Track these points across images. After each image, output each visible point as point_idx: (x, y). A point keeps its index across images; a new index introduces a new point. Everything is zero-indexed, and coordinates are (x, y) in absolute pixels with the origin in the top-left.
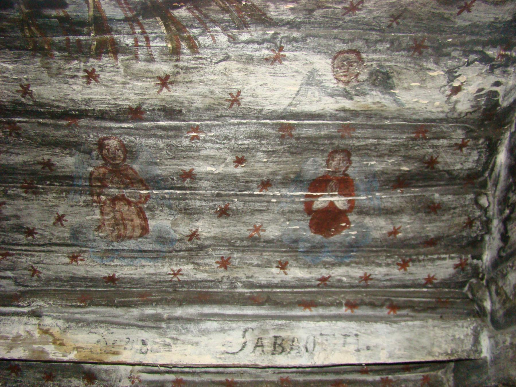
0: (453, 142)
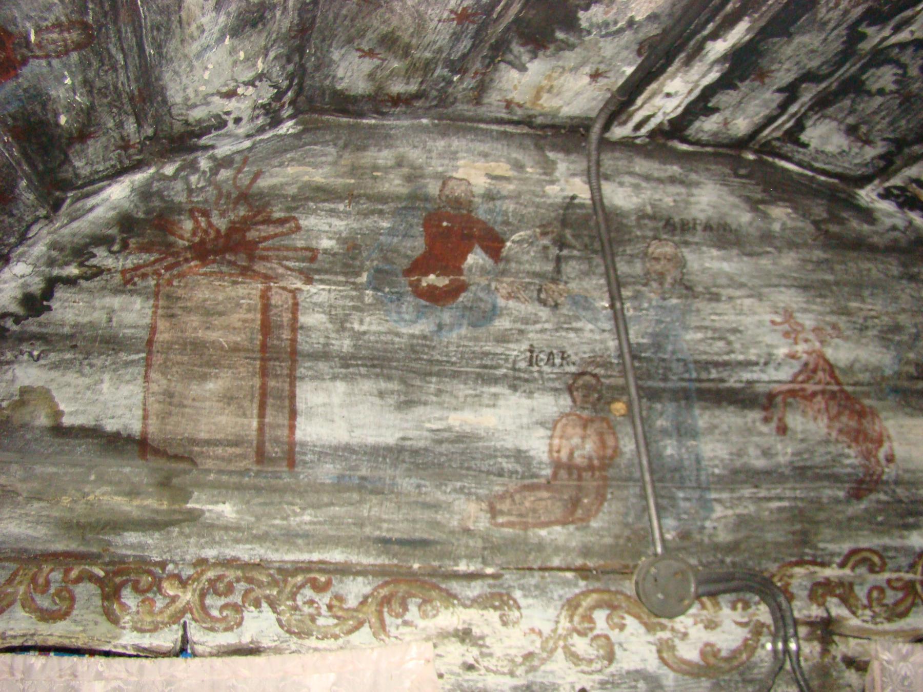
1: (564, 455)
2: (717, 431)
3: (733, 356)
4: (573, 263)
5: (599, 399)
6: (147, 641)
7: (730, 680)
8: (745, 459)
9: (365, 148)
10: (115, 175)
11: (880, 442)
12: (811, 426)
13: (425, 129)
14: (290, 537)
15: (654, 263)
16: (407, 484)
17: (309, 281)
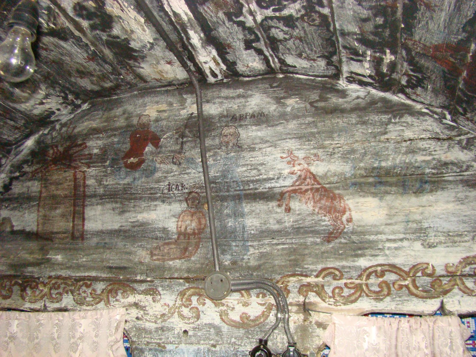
0: (16, 125)
1: (183, 229)
2: (254, 213)
3: (261, 176)
4: (188, 144)
5: (198, 203)
6: (33, 306)
7: (254, 330)
8: (268, 225)
9: (112, 109)
10: (27, 137)
11: (344, 212)
12: (304, 207)
13: (136, 96)
14: (79, 267)
15: (224, 138)
16: (120, 244)
17: (89, 167)
